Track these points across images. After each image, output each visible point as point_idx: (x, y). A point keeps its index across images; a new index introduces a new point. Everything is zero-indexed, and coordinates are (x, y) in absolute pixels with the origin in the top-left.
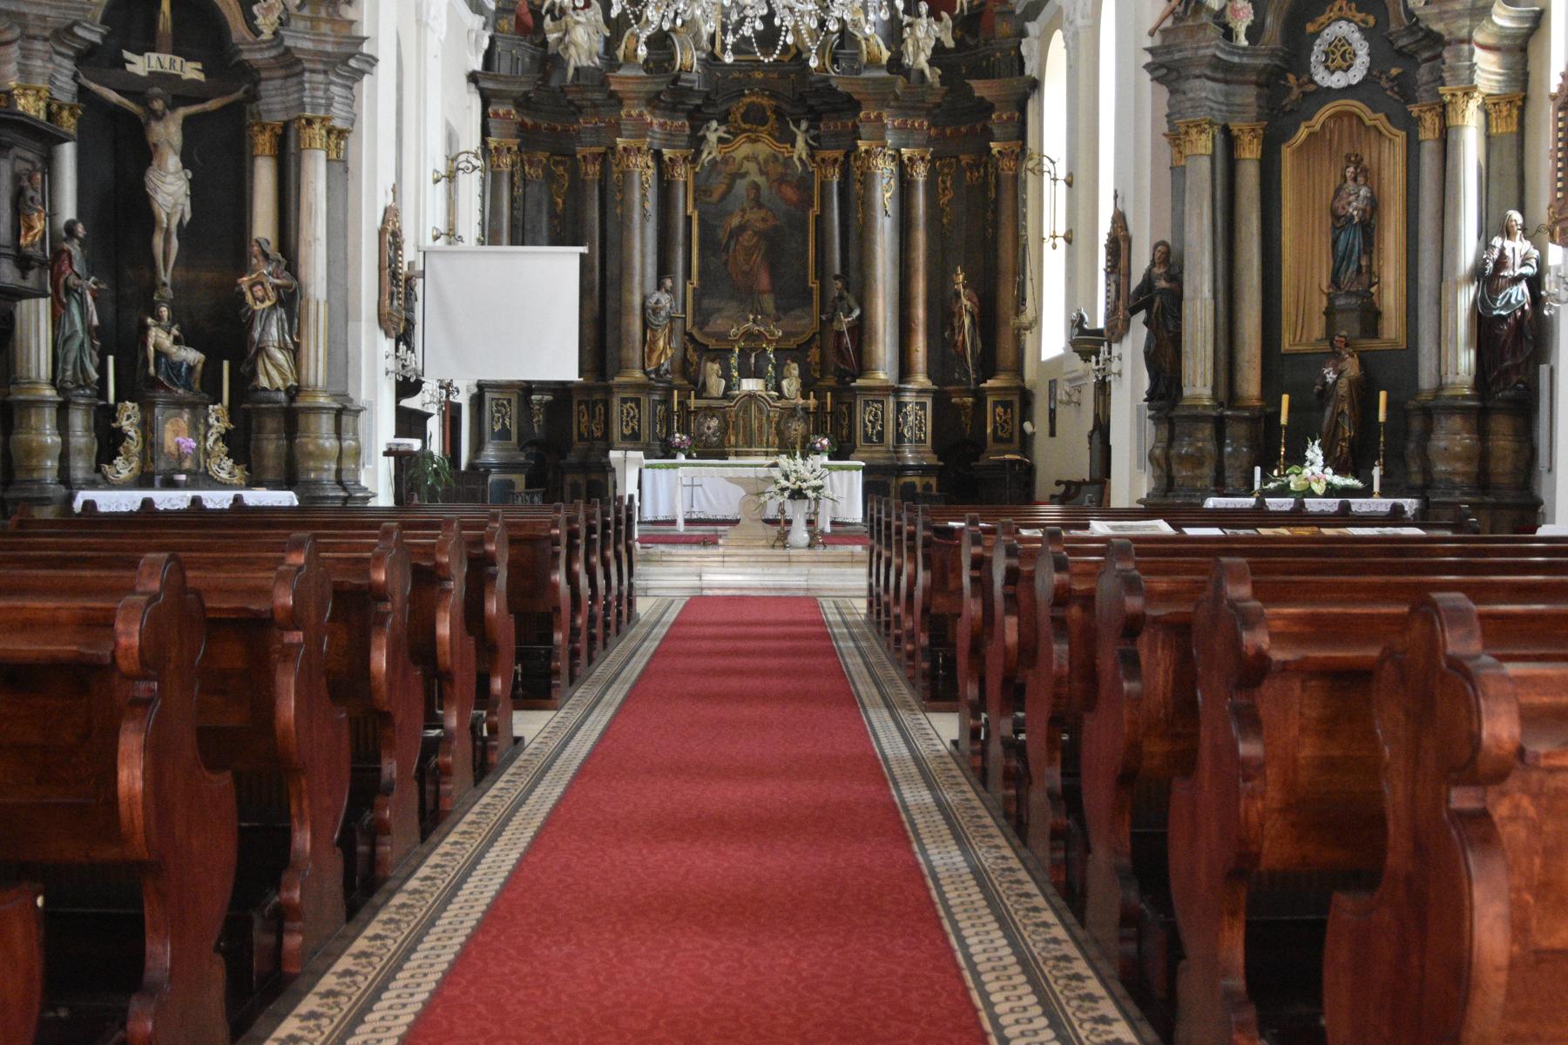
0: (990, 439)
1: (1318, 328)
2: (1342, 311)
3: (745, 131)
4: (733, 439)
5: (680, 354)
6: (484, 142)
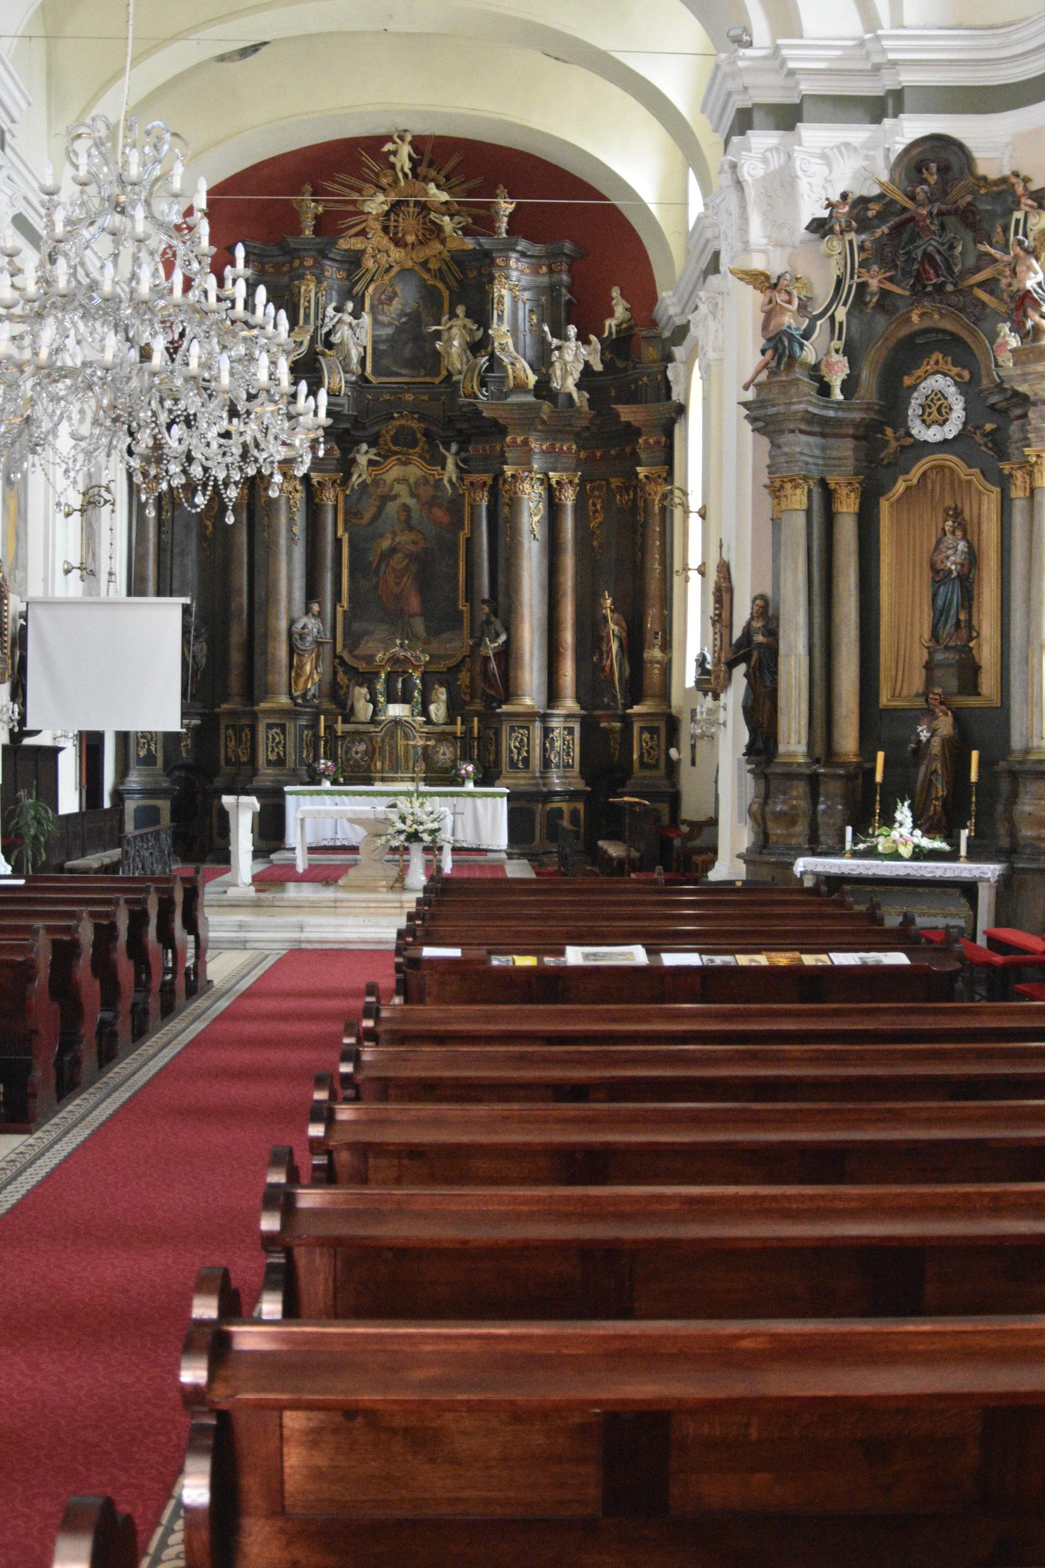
0: (636, 765)
1: (918, 682)
2: (941, 665)
3: (396, 453)
4: (379, 764)
5: (328, 678)
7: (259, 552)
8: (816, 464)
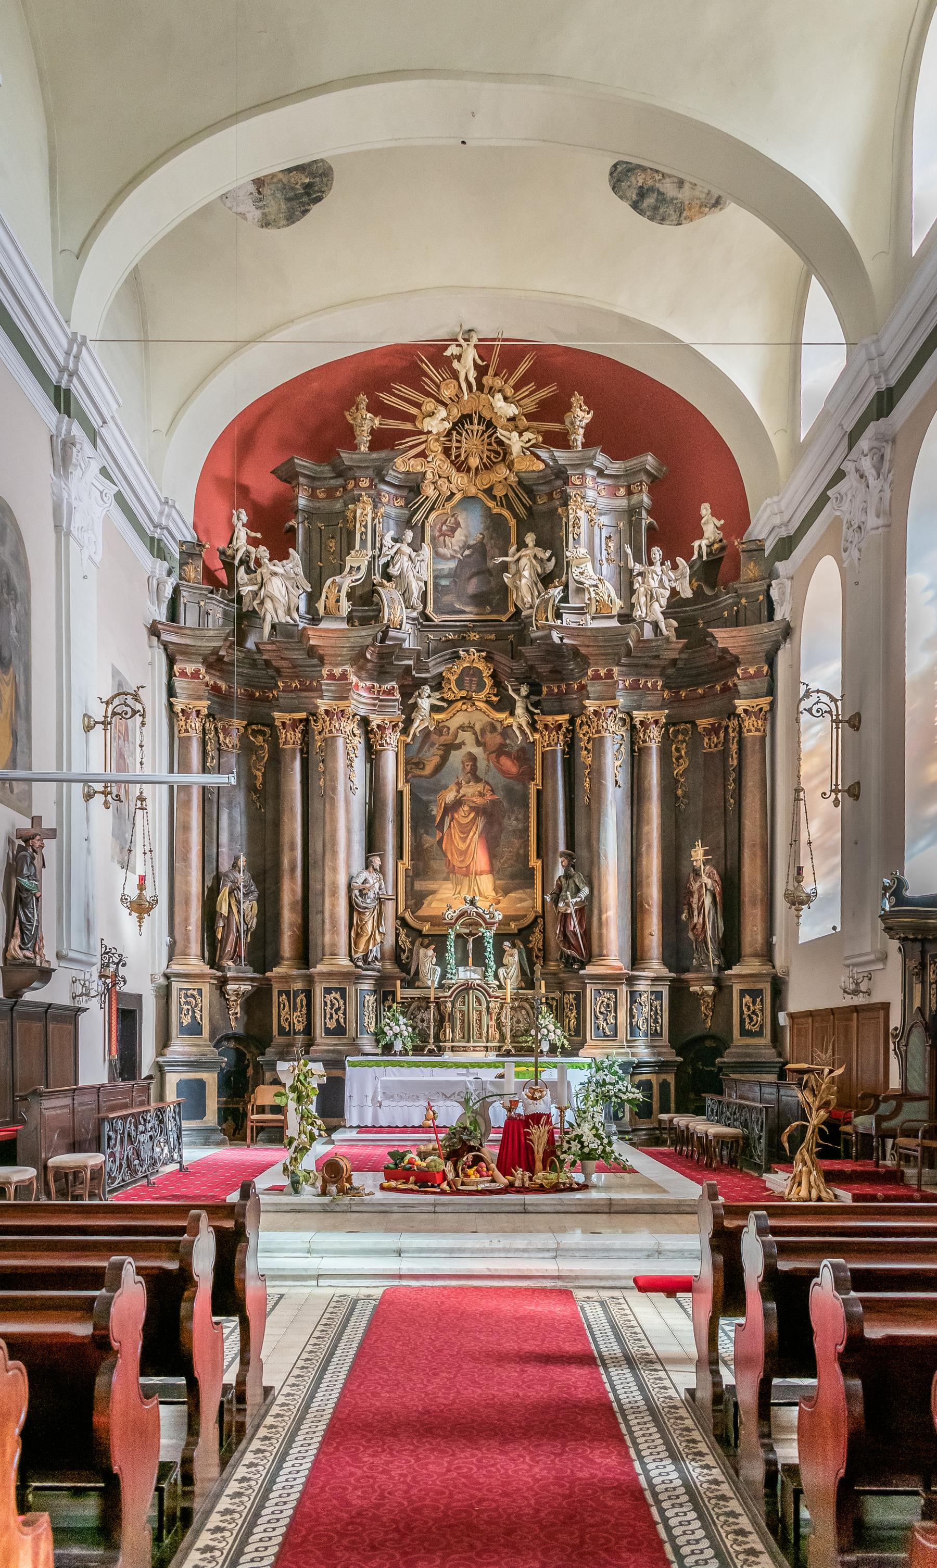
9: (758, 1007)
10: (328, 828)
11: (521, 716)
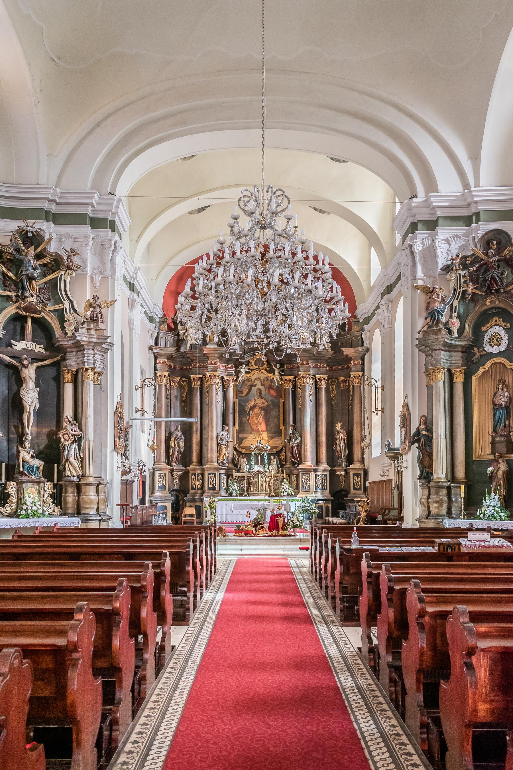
1: (488, 450)
2: (499, 442)
6: (155, 374)
7: (205, 408)
8: (447, 363)
9: (359, 480)
10: (210, 416)
11: (277, 376)
